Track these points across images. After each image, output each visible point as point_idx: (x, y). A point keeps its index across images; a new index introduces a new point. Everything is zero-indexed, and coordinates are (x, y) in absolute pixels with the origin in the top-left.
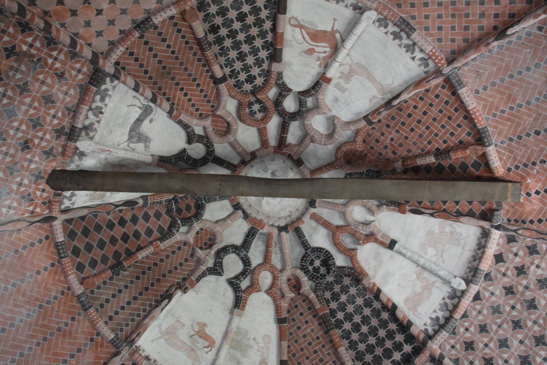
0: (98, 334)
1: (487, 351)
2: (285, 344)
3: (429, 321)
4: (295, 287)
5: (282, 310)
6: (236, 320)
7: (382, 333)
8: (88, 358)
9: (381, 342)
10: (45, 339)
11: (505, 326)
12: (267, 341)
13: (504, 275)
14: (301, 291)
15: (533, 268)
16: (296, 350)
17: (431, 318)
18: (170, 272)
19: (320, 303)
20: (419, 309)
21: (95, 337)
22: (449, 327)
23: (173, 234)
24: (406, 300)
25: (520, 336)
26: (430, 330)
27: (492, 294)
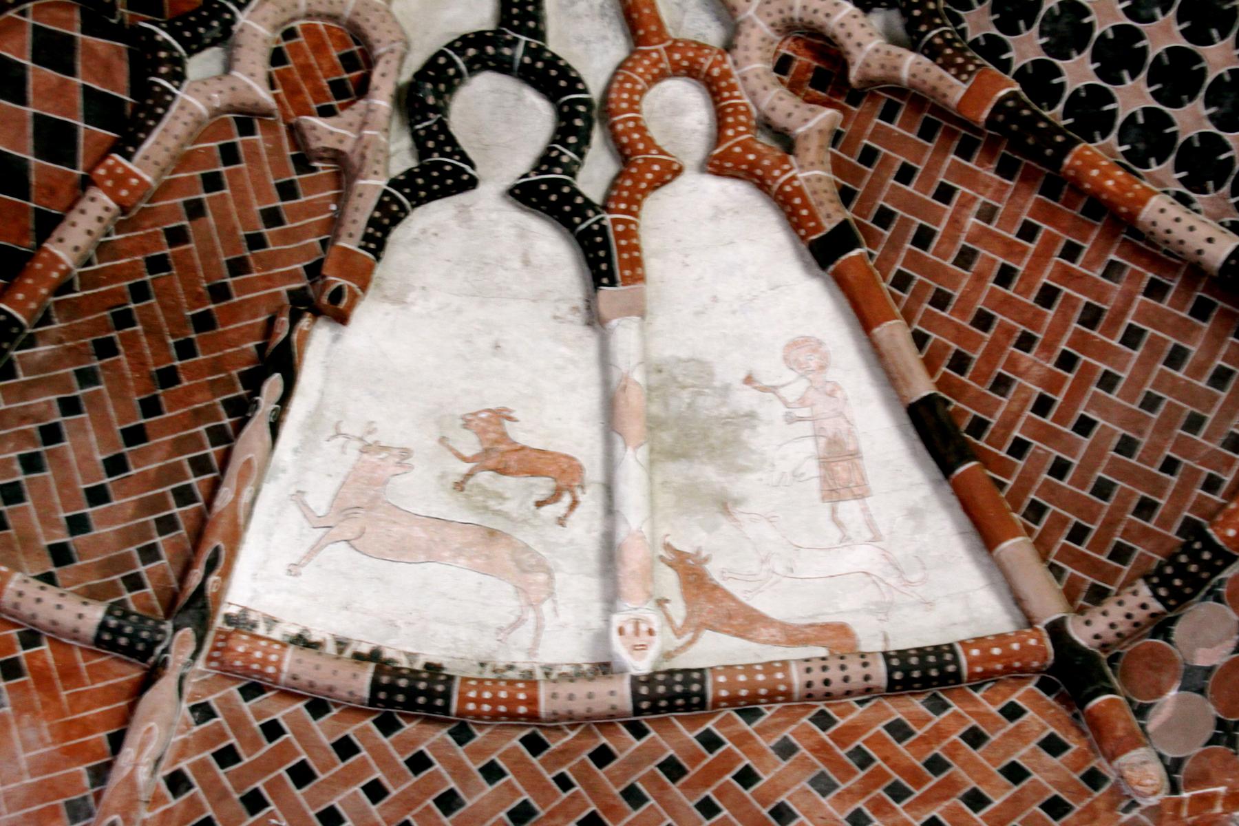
2: (894, 333)
4: (819, 80)
5: (812, 200)
8: (27, 747)
12: (813, 365)
14: (854, 75)
16: (960, 334)
18: (239, 266)
19: (960, 71)
23: (164, 100)
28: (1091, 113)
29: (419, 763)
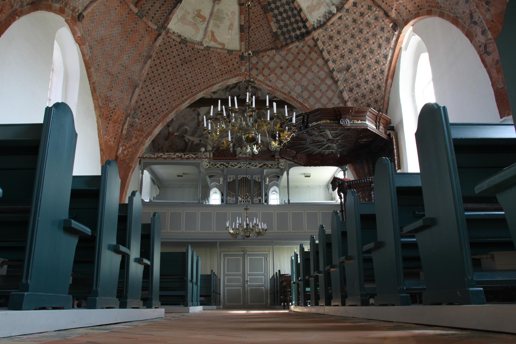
0: (149, 27)
1: (337, 42)
2: (243, 17)
3: (316, 21)
6: (216, 7)
7: (293, 20)
9: (291, 24)
10: (127, 37)
11: (348, 35)
13: (355, 13)
15: (367, 16)
17: (317, 20)
20: (313, 14)
21: (147, 29)
22: (324, 28)
24: (308, 7)
25: (352, 42)
26: (316, 25)
27: (347, 19)
28: (272, 10)
29: (182, 48)
